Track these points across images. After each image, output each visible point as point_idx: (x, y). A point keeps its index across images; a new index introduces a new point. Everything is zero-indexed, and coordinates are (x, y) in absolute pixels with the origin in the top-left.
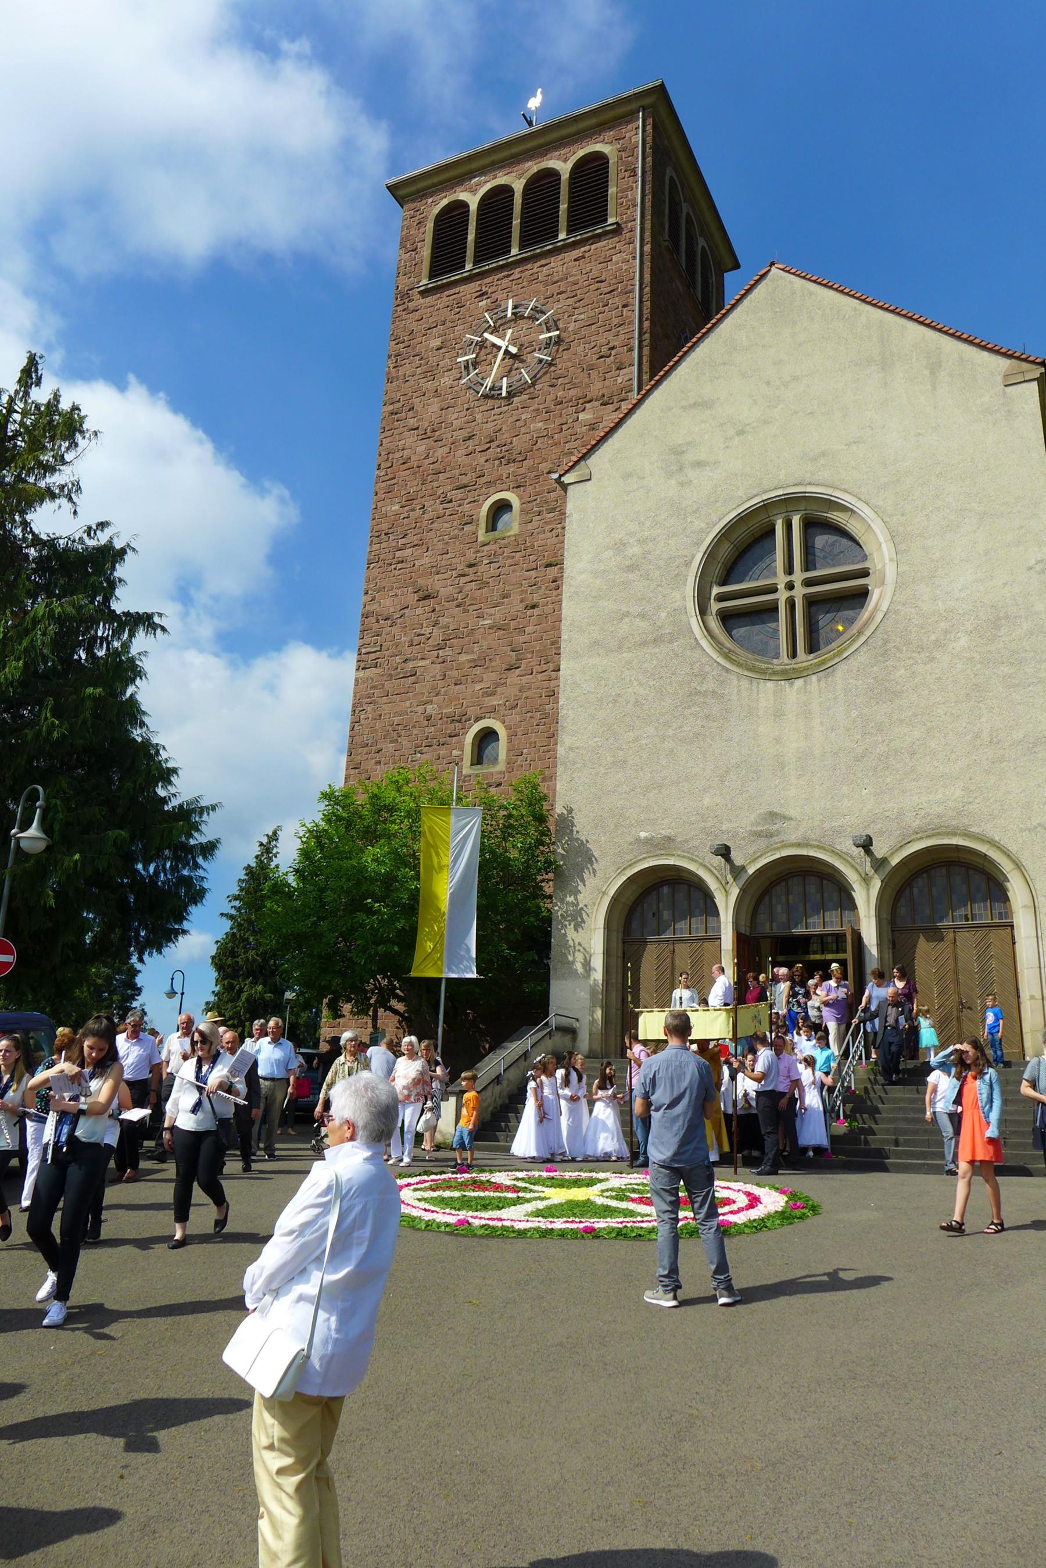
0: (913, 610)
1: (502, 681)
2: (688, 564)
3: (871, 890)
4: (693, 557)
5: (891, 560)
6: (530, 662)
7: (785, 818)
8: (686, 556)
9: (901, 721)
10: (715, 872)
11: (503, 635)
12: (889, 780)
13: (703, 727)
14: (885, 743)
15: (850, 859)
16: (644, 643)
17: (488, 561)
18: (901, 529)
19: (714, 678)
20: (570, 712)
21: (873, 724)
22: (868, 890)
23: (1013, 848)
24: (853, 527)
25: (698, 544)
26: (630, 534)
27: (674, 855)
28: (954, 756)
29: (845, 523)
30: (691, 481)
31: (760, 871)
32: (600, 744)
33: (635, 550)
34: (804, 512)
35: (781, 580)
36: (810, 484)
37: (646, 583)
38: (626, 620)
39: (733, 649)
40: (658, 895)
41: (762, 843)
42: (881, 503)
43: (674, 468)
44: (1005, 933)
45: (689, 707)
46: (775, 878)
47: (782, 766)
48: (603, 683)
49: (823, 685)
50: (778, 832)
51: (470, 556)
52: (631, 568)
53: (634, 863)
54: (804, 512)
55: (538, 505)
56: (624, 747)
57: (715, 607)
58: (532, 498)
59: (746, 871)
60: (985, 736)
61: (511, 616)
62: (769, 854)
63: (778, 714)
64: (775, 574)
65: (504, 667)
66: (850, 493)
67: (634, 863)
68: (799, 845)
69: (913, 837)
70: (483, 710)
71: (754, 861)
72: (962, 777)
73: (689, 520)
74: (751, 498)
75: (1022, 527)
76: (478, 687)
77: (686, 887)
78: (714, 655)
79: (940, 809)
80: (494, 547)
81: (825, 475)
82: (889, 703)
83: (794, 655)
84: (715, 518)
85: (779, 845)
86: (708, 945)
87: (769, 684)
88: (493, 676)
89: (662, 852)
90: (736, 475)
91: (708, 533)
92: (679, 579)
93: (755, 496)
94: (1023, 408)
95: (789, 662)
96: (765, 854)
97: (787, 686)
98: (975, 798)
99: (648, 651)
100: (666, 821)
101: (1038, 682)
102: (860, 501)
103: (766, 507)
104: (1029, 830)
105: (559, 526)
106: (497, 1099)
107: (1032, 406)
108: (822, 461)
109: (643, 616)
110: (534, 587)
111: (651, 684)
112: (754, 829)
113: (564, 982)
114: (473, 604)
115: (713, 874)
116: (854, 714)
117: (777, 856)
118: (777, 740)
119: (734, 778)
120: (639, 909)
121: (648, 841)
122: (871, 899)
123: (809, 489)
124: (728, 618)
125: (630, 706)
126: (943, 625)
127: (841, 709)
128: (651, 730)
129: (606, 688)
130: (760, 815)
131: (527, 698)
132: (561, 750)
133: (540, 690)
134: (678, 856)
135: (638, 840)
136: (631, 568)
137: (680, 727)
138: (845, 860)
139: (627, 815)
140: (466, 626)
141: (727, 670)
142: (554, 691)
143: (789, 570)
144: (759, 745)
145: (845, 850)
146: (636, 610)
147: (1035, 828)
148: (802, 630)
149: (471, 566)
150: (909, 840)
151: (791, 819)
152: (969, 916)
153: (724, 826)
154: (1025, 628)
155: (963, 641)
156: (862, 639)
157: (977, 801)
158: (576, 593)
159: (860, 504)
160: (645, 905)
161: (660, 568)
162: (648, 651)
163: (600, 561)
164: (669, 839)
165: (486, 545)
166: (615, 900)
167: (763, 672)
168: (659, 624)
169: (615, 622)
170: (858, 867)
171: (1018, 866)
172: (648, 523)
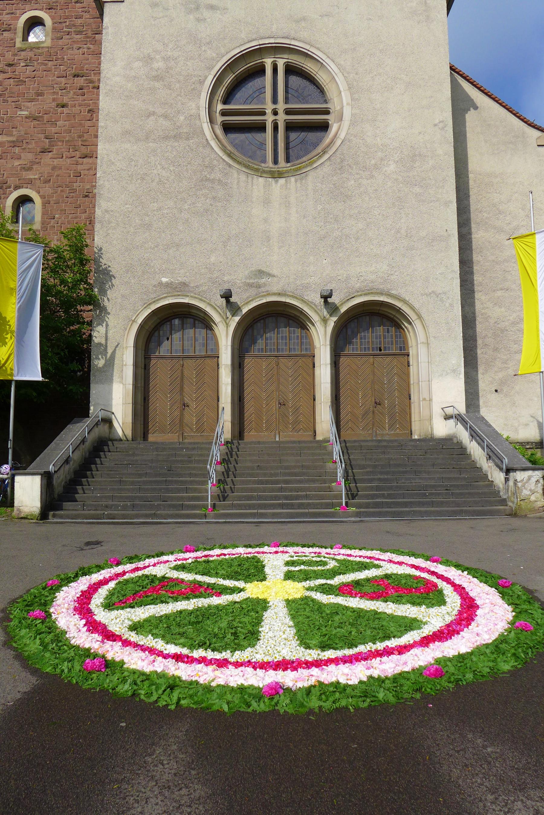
0: (361, 141)
1: (37, 160)
2: (202, 82)
3: (328, 328)
4: (206, 77)
5: (348, 104)
6: (61, 149)
7: (269, 275)
8: (200, 76)
9: (351, 216)
10: (219, 310)
11: (38, 124)
12: (341, 255)
13: (211, 205)
14: (339, 230)
15: (313, 306)
16: (166, 138)
17: (24, 64)
18: (355, 83)
19: (220, 170)
20: (106, 183)
21: (332, 216)
22: (326, 327)
23: (416, 306)
24: (321, 77)
25: (210, 68)
26: (156, 51)
27: (188, 296)
28: (383, 243)
29: (315, 73)
30: (205, 19)
31: (251, 311)
32: (130, 210)
33: (159, 64)
34: (287, 60)
35: (269, 107)
36: (294, 39)
37: (169, 92)
38: (152, 118)
39: (233, 151)
40: (171, 325)
41: (253, 292)
42: (342, 63)
43: (193, 6)
44: (403, 359)
45: (201, 189)
46: (258, 317)
47: (268, 239)
48: (133, 163)
49: (299, 185)
50: (265, 285)
51: (9, 56)
52: (157, 78)
53: (157, 300)
54: (219, 102)
55: (67, 27)
56: (150, 213)
57: (220, 119)
58: (62, 20)
59: (241, 311)
60: (403, 232)
61: (45, 110)
62: (258, 299)
63: (267, 202)
64: (263, 102)
65: (39, 150)
66: (322, 51)
67: (157, 300)
68: (279, 294)
69: (356, 294)
70: (21, 181)
71: (247, 303)
72: (388, 257)
73: (203, 49)
74: (251, 41)
75: (432, 97)
76: (17, 163)
77: (192, 320)
78: (221, 153)
79: (373, 277)
80: (31, 54)
81: (304, 34)
82: (343, 203)
83: (276, 162)
84: (223, 51)
85: (265, 293)
86: (208, 361)
87: (261, 180)
88: (30, 156)
89: (179, 293)
90: (240, 21)
91: (218, 61)
92: (195, 93)
93: (254, 40)
94: (436, 16)
95: (274, 166)
96: (255, 299)
97: (273, 182)
98: (395, 272)
99: (170, 144)
100: (182, 271)
101: (437, 201)
102: (328, 59)
103: (262, 51)
104: (426, 294)
105: (85, 46)
106: (67, 476)
107: (442, 16)
108: (303, 24)
109: (165, 117)
110: (64, 91)
111: (172, 168)
112: (248, 281)
113: (101, 386)
114: (11, 97)
115: (217, 311)
116: (319, 207)
117: (264, 301)
118: (266, 220)
119: (234, 244)
120: (156, 334)
121: (168, 285)
122: (327, 334)
123: (293, 42)
124: (228, 128)
125: (154, 184)
126: (380, 154)
127: (311, 203)
128: (171, 204)
129: (136, 168)
130: (252, 271)
131: (58, 176)
132: (98, 212)
133: (68, 171)
134: (192, 297)
135: (161, 283)
136: (157, 78)
137: (194, 203)
138: (311, 306)
139: (152, 265)
140: (6, 113)
141: (230, 166)
142: (80, 173)
143: (275, 101)
144: (252, 223)
145: (310, 300)
146: (160, 111)
147: (430, 294)
148: (283, 145)
149: (10, 65)
150: (353, 296)
151: (274, 276)
152: (382, 349)
153: (226, 277)
154: (430, 164)
155: (392, 167)
156: (326, 156)
157: (396, 274)
158: (111, 91)
159: (328, 61)
160: (161, 332)
161: (179, 82)
162: (170, 144)
163: (132, 69)
164: (184, 284)
165: (23, 50)
166: (142, 327)
167: (257, 170)
168: (178, 124)
169: (143, 118)
170: (319, 312)
171: (420, 317)
172: (171, 46)
